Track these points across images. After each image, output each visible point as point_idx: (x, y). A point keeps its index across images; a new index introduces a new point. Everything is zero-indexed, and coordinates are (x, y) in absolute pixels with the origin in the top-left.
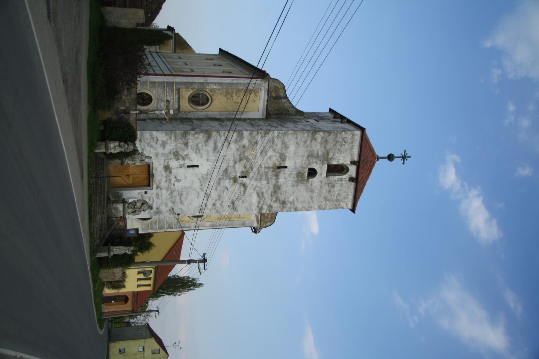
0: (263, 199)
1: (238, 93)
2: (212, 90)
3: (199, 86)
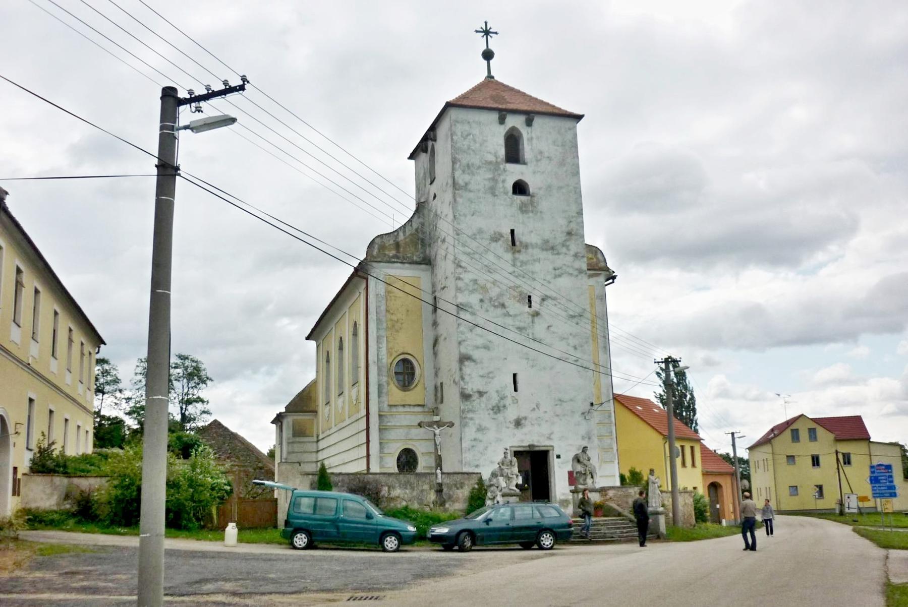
0: (564, 268)
1: (391, 312)
2: (389, 353)
3: (384, 374)
